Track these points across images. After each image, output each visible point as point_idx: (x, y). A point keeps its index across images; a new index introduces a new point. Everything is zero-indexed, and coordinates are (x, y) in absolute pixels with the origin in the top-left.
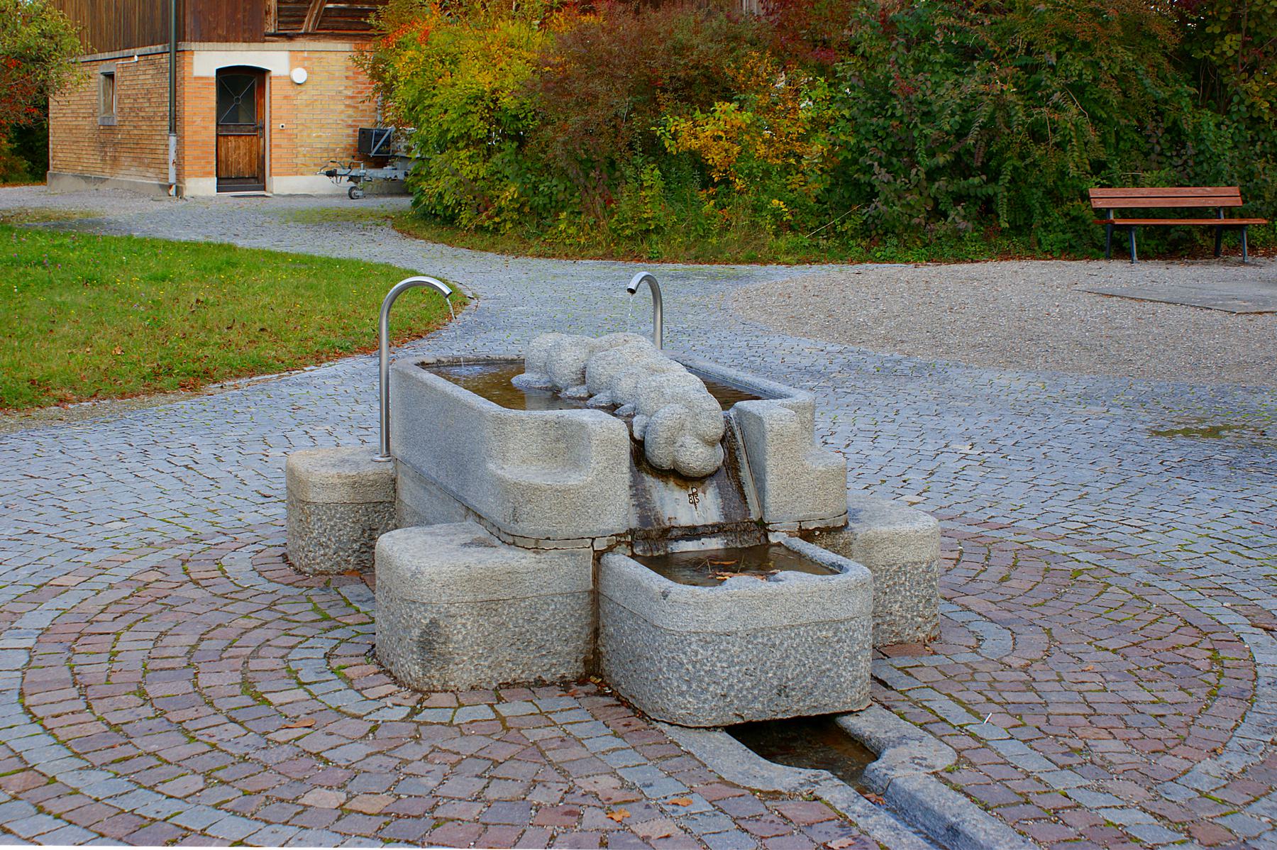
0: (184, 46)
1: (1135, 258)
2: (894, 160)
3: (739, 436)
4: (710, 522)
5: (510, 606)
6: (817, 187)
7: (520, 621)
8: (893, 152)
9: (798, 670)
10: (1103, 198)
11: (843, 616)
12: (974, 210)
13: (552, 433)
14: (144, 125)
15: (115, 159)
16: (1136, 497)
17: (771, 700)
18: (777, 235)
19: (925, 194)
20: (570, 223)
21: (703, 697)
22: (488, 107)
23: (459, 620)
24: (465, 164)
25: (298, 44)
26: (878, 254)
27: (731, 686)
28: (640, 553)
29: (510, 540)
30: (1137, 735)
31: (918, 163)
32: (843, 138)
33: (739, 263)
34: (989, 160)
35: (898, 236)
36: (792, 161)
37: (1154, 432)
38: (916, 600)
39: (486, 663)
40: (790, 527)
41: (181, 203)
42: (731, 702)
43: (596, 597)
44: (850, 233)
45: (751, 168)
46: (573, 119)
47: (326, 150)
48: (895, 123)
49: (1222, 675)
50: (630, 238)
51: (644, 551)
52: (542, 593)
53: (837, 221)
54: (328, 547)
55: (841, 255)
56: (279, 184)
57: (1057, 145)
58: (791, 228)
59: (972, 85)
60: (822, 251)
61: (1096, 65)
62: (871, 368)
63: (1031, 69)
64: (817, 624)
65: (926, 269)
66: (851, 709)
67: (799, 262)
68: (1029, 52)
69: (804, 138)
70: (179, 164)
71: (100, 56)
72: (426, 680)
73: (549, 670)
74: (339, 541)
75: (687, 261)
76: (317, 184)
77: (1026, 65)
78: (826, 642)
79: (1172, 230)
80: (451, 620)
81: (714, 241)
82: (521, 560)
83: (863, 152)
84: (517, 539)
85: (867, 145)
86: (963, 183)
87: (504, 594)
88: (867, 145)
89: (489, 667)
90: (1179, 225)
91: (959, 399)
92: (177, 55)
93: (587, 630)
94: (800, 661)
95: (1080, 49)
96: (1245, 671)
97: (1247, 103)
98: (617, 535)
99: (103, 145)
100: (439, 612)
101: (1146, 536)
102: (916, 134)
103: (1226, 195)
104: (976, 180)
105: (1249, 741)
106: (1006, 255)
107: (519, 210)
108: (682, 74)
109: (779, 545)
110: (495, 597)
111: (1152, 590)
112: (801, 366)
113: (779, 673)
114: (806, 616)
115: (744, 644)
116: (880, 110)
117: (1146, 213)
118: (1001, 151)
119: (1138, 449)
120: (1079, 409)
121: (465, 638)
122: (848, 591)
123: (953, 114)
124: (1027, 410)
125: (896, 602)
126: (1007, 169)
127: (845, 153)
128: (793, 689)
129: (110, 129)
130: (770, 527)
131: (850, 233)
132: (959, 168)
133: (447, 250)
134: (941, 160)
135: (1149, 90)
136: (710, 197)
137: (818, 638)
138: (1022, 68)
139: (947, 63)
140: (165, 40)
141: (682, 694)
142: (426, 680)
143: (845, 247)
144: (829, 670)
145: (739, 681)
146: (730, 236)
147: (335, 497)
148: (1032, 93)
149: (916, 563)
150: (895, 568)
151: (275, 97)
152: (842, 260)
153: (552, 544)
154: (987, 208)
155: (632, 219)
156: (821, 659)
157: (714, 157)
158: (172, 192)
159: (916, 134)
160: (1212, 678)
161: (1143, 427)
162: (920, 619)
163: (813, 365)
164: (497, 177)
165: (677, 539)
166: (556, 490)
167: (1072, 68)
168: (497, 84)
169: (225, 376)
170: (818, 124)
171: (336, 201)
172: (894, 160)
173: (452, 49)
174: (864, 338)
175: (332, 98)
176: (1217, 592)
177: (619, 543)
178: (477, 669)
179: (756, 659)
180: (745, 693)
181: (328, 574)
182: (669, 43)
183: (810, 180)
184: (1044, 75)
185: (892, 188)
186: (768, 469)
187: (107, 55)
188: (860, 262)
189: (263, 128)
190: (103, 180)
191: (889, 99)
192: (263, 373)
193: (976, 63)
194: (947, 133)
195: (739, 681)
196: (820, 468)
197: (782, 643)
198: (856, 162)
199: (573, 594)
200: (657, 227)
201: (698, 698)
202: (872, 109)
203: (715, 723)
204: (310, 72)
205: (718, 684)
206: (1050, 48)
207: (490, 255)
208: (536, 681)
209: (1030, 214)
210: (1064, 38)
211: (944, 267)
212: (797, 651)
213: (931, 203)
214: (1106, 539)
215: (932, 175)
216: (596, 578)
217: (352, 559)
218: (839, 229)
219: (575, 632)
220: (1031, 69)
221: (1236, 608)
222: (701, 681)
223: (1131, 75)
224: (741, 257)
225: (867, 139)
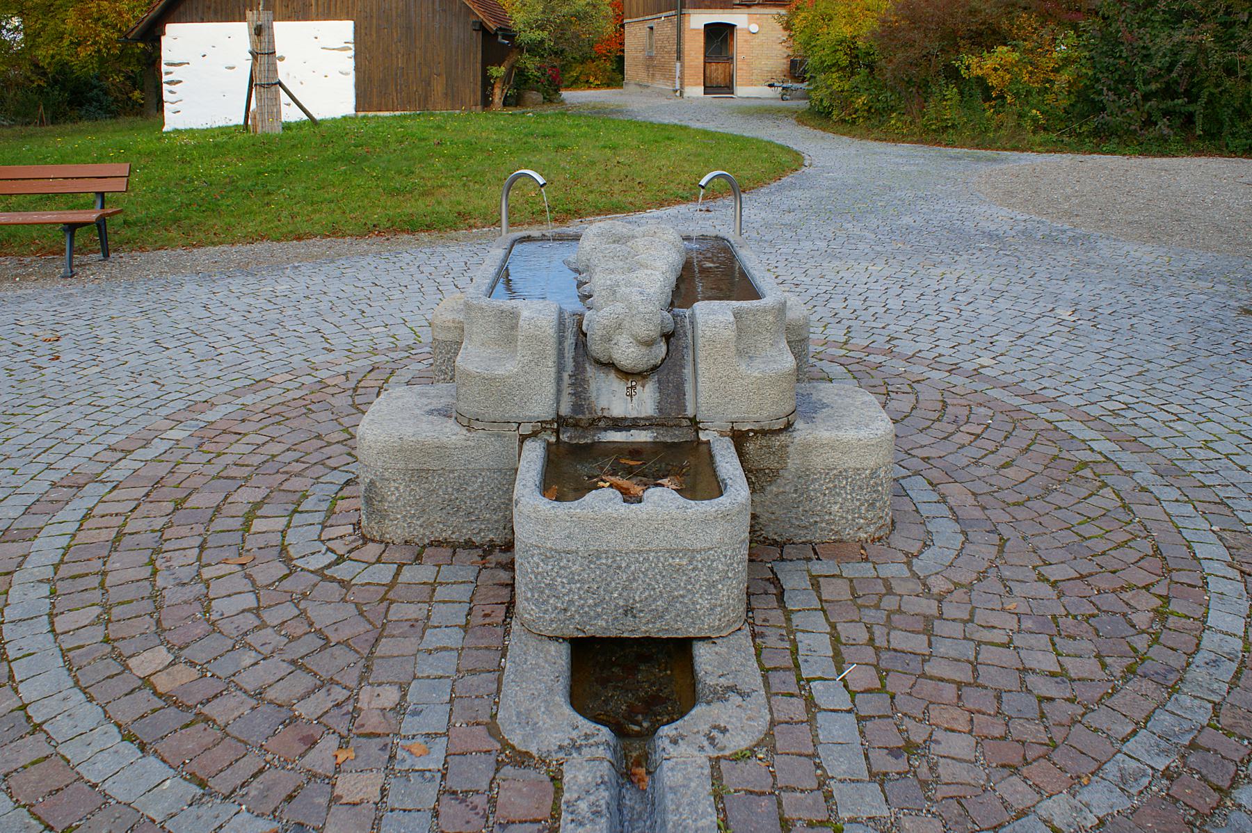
0: (684, 11)
2: (1120, 86)
3: (690, 337)
4: (643, 415)
5: (440, 476)
6: (1065, 103)
7: (450, 490)
8: (1120, 81)
9: (647, 593)
11: (699, 546)
12: (1178, 122)
13: (507, 321)
14: (666, 56)
15: (653, 75)
16: (1190, 379)
17: (616, 619)
18: (1034, 132)
19: (1141, 109)
20: (899, 120)
21: (544, 607)
22: (849, 47)
23: (392, 484)
24: (835, 81)
25: (754, 10)
27: (571, 602)
28: (566, 440)
31: (1137, 89)
32: (1084, 71)
33: (1006, 150)
34: (1193, 87)
35: (1119, 137)
36: (1047, 85)
37: (1245, 310)
38: (858, 504)
39: (418, 523)
40: (721, 427)
41: (680, 100)
42: (572, 617)
45: (1018, 89)
46: (900, 55)
47: (770, 72)
48: (1121, 61)
49: (1156, 640)
50: (934, 131)
51: (570, 438)
52: (470, 467)
53: (1076, 126)
55: (1078, 149)
56: (741, 91)
57: (1244, 77)
58: (1045, 129)
59: (1178, 36)
60: (1065, 145)
62: (1039, 236)
63: (1227, 25)
64: (669, 551)
65: (1138, 160)
66: (708, 635)
67: (1047, 151)
68: (1227, 13)
69: (1056, 70)
70: (682, 78)
71: (647, 18)
73: (478, 533)
75: (971, 147)
76: (763, 91)
77: (1226, 22)
78: (679, 569)
80: (386, 483)
83: (1098, 80)
85: (1101, 76)
86: (1170, 103)
87: (434, 465)
88: (1101, 76)
89: (421, 526)
91: (1093, 266)
92: (681, 15)
94: (649, 585)
96: (1186, 637)
98: (542, 422)
99: (648, 67)
101: (1179, 426)
102: (1136, 69)
104: (1180, 101)
105: (1134, 764)
106: (1199, 153)
107: (869, 111)
108: (974, 28)
110: (425, 467)
111: (1146, 497)
112: (987, 230)
113: (625, 594)
114: (657, 542)
115: (586, 563)
118: (1202, 82)
119: (1220, 326)
120: (1188, 284)
121: (398, 500)
122: (705, 521)
123: (1165, 55)
124: (1141, 281)
125: (835, 503)
126: (1205, 94)
127: (1086, 81)
128: (642, 611)
129: (651, 58)
132: (1168, 92)
133: (819, 133)
134: (1154, 87)
136: (991, 107)
137: (670, 565)
138: (1221, 24)
139: (1165, 21)
140: (676, 9)
143: (1082, 143)
144: (682, 596)
145: (580, 598)
146: (1002, 132)
149: (858, 470)
150: (835, 472)
151: (739, 41)
153: (480, 425)
154: (1189, 119)
155: (936, 119)
156: (673, 585)
157: (993, 81)
158: (678, 94)
160: (1141, 643)
161: (1237, 304)
162: (862, 521)
163: (997, 230)
164: (856, 89)
165: (605, 430)
166: (484, 378)
168: (855, 34)
169: (589, 215)
170: (1067, 61)
171: (773, 102)
172: (1120, 86)
173: (831, 12)
174: (1050, 211)
175: (773, 41)
176: (1213, 508)
177: (544, 429)
178: (410, 527)
179: (598, 579)
180: (587, 609)
182: (967, 8)
183: (1059, 98)
184: (1237, 30)
185: (1117, 105)
187: (650, 17)
188: (1090, 154)
189: (732, 58)
190: (648, 87)
192: (617, 213)
193: (1184, 21)
194: (1160, 69)
195: (580, 598)
196: (756, 374)
197: (628, 566)
198: (1093, 87)
199: (500, 470)
200: (953, 125)
201: (539, 608)
202: (1107, 51)
203: (554, 634)
204: (761, 26)
205: (558, 598)
206: (1243, 10)
207: (844, 138)
208: (466, 542)
209: (1222, 124)
211: (1150, 160)
212: (646, 575)
213: (1145, 116)
214: (1136, 425)
215: (1146, 97)
218: (1078, 130)
219: (503, 503)
220: (1227, 25)
221: (1223, 534)
222: (542, 592)
224: (1008, 146)
225: (1101, 72)
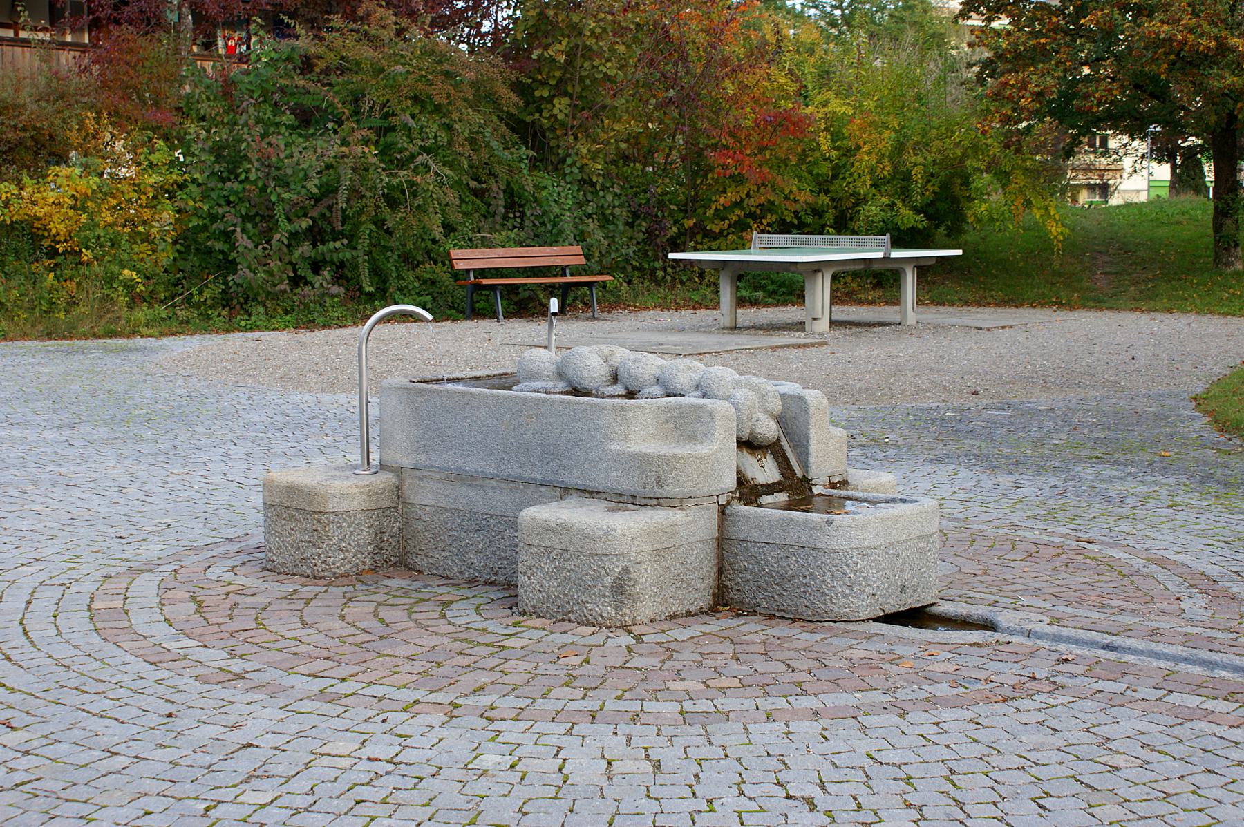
1: (501, 317)
10: (466, 259)
26: (243, 323)
29: (655, 502)
30: (808, 677)
43: (722, 542)
44: (209, 302)
52: (690, 540)
54: (347, 551)
61: (449, 128)
72: (619, 617)
74: (358, 545)
79: (520, 290)
80: (638, 566)
81: (62, 315)
82: (677, 516)
84: (661, 501)
90: (526, 284)
93: (715, 570)
95: (432, 112)
97: (578, 165)
100: (629, 561)
103: (567, 254)
109: (820, 495)
110: (664, 546)
116: (233, 174)
117: (498, 273)
130: (813, 482)
131: (209, 302)
135: (496, 152)
141: (845, 597)
142: (619, 617)
147: (355, 504)
148: (392, 158)
152: (206, 330)
159: (274, 198)
166: (696, 458)
167: (428, 130)
181: (349, 575)
186: (811, 436)
191: (241, 163)
199: (706, 540)
210: (416, 99)
216: (720, 526)
217: (367, 561)
223: (480, 137)
